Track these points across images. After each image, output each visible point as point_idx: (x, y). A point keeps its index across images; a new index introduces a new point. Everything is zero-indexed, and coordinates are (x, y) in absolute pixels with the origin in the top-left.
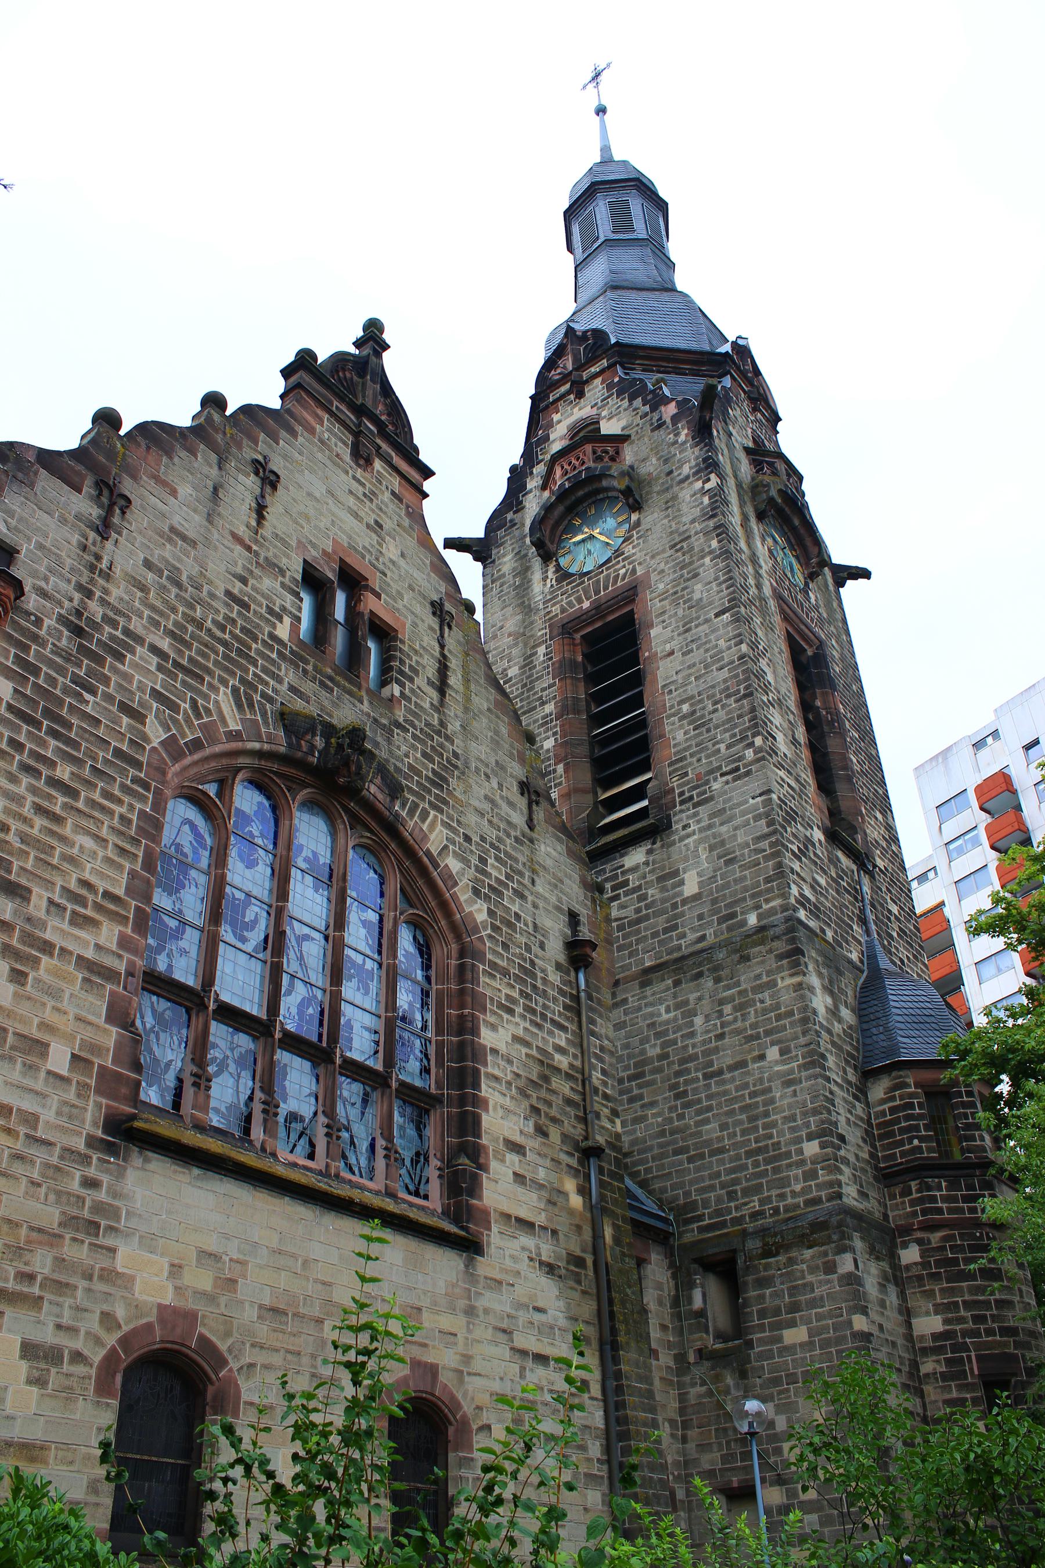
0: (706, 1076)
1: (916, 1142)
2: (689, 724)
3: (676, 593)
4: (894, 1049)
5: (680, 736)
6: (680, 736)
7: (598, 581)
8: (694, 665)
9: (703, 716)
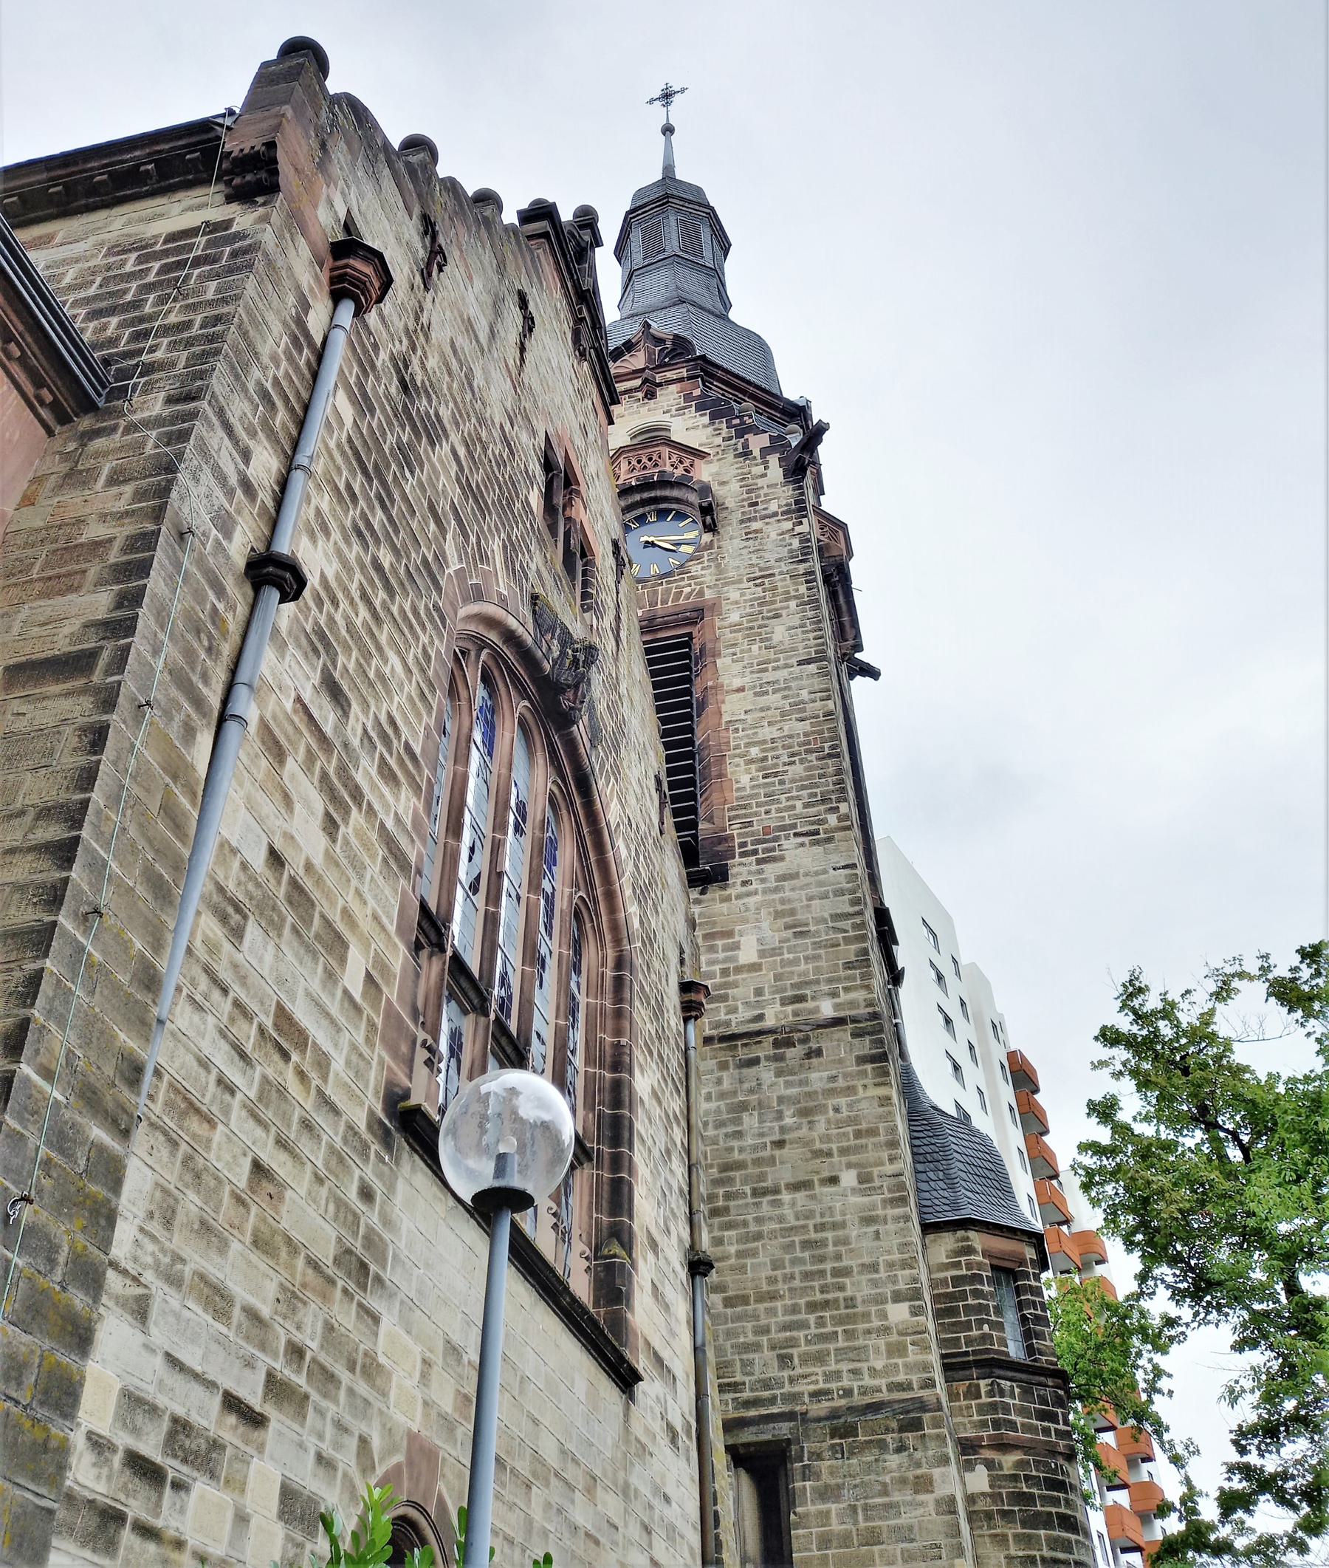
0: (755, 1193)
1: (986, 1327)
2: (758, 771)
3: (751, 628)
4: (955, 1206)
5: (745, 780)
6: (745, 780)
7: (656, 592)
8: (769, 708)
9: (775, 765)
